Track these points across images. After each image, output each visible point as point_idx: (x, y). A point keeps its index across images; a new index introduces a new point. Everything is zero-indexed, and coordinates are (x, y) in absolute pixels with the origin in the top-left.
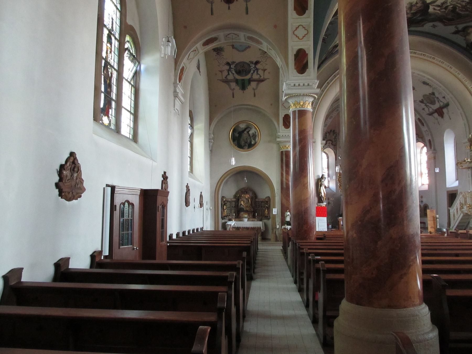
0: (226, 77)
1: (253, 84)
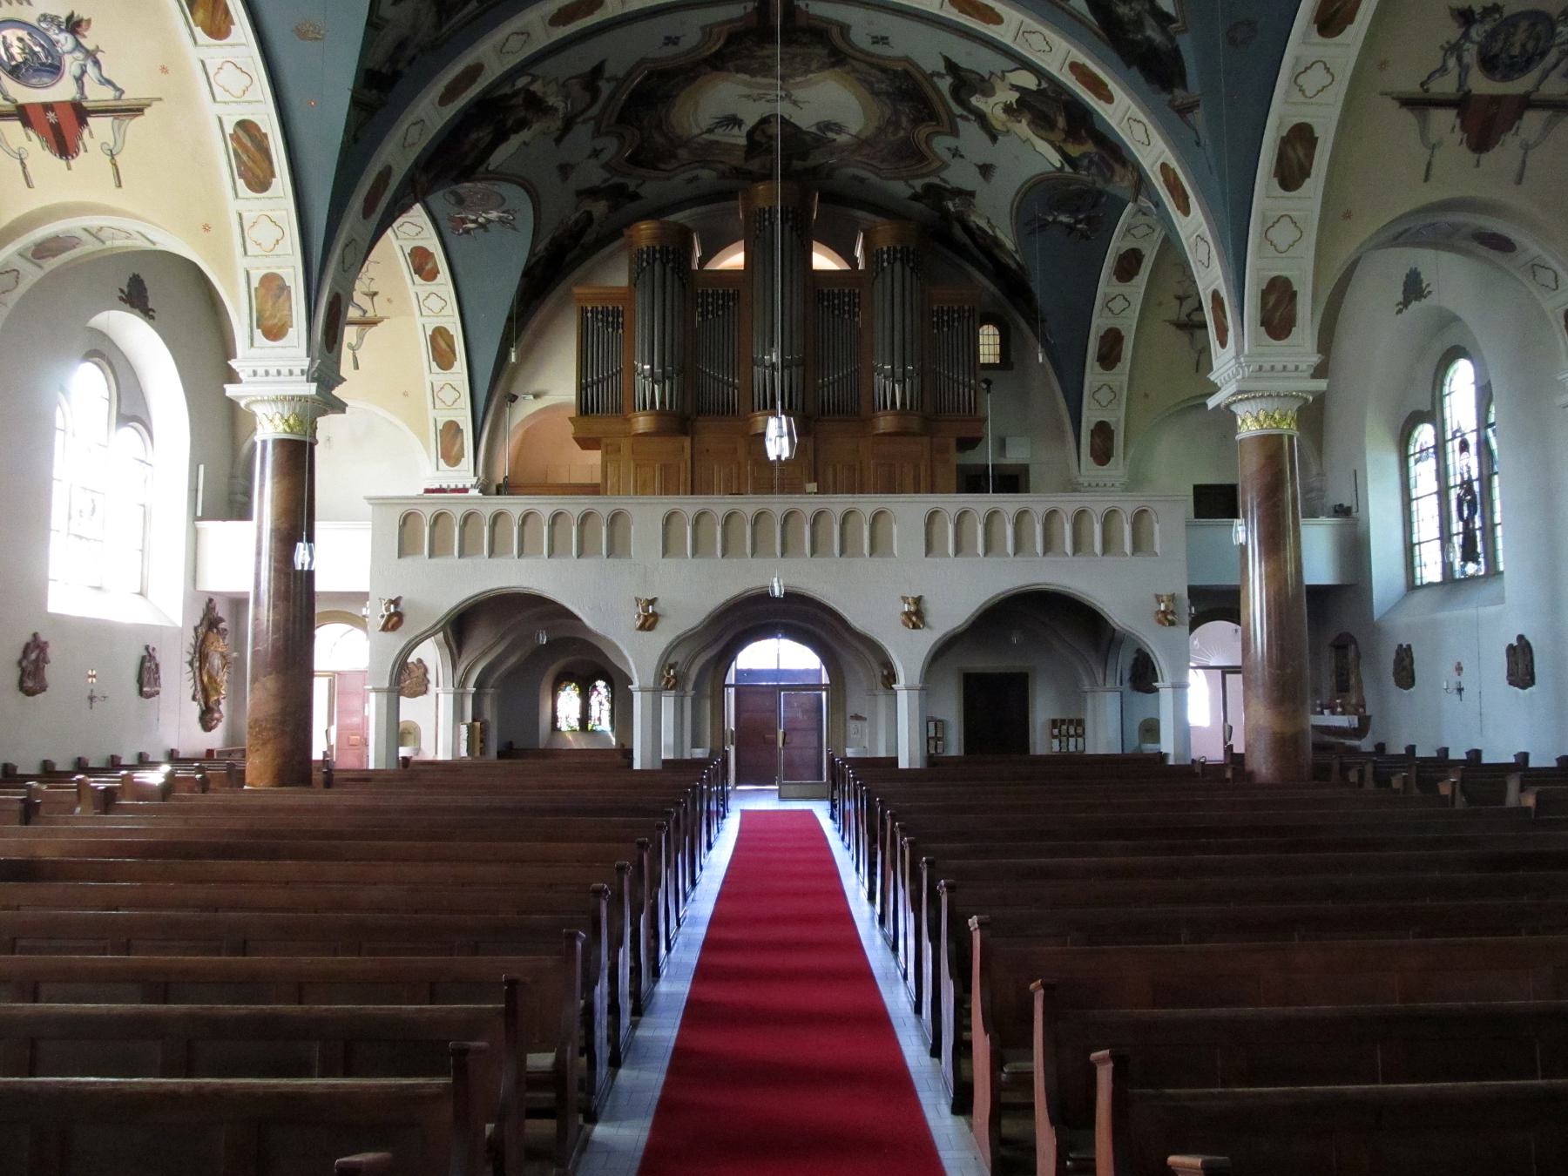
0: (1188, 315)
1: (99, 127)
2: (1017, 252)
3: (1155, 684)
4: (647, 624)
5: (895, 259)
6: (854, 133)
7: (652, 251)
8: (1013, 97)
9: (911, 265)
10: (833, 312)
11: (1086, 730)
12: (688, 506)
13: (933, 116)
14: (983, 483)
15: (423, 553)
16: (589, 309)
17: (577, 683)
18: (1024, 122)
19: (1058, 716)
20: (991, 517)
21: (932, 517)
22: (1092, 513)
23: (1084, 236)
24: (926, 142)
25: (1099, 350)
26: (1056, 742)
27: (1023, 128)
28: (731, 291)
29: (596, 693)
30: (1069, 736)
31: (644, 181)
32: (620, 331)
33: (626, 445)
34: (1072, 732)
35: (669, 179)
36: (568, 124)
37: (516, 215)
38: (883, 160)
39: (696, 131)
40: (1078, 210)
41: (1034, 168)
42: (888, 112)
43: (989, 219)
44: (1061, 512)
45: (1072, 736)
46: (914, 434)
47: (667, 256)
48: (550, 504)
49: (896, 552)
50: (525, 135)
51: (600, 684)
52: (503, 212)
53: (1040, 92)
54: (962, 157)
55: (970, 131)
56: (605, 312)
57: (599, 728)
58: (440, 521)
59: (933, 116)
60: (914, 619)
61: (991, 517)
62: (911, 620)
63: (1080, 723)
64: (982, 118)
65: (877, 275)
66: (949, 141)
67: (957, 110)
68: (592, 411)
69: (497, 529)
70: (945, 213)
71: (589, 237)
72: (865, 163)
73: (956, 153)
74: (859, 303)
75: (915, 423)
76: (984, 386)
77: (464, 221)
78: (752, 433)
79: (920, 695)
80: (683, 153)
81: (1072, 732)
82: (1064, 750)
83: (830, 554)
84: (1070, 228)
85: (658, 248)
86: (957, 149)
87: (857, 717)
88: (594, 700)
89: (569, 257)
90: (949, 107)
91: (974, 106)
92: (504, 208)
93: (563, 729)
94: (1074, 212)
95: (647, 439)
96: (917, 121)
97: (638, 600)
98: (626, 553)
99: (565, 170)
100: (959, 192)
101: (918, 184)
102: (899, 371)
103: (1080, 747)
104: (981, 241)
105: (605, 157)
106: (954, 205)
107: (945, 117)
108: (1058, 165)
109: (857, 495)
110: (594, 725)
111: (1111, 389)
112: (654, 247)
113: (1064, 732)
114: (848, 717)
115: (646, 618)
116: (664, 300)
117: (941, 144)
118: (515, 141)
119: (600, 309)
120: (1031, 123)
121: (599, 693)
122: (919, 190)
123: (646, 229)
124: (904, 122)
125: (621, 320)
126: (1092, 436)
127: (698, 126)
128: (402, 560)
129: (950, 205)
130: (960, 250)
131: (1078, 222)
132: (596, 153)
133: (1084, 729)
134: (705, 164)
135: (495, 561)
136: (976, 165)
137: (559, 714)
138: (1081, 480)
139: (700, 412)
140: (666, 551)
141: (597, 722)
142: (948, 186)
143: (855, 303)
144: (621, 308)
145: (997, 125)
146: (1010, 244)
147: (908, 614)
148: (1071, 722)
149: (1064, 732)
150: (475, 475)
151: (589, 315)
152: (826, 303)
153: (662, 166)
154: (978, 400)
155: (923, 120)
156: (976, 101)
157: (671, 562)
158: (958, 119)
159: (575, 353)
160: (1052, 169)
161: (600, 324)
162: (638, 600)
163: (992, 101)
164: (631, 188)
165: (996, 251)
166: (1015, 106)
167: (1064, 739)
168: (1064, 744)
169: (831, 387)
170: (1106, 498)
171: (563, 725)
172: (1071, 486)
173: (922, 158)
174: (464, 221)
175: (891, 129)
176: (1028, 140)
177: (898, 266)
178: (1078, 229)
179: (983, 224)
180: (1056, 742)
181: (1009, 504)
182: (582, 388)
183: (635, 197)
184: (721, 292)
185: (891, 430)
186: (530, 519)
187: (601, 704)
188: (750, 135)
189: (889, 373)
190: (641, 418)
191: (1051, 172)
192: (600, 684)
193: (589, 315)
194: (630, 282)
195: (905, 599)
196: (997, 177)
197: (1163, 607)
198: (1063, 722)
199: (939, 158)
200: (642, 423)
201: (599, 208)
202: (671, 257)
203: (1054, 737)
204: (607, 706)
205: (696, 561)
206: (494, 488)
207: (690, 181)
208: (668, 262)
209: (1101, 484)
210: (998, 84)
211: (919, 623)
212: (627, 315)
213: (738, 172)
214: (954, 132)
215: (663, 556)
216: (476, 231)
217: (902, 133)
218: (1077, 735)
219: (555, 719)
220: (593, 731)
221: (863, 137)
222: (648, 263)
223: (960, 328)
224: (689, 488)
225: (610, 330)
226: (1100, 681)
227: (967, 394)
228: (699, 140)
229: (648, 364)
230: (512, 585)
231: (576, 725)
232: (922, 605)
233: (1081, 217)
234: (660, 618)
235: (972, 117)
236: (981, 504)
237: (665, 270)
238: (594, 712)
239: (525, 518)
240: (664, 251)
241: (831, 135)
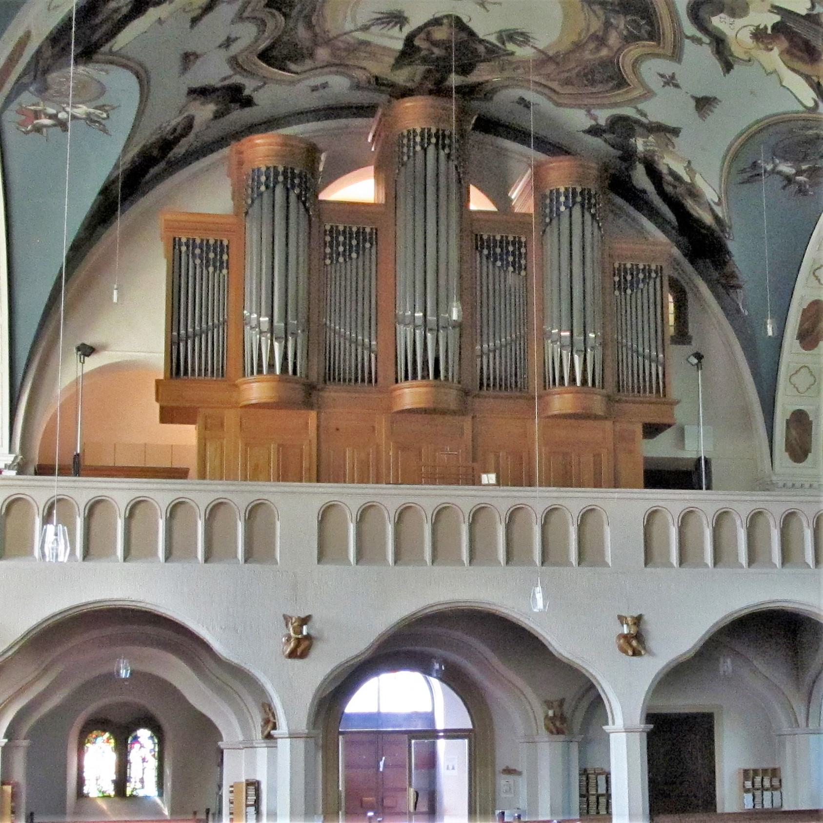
2: (719, 204)
3: (605, 727)
4: (299, 651)
5: (574, 203)
6: (541, 47)
9: (593, 211)
11: (783, 781)
13: (654, 35)
14: (695, 479)
15: (115, 553)
16: (184, 240)
17: (112, 733)
18: (776, 51)
19: (751, 766)
21: (326, 514)
22: (701, 514)
23: (802, 191)
25: (801, 325)
26: (748, 797)
28: (368, 230)
29: (137, 746)
30: (763, 789)
31: (265, 83)
32: (225, 271)
34: (767, 783)
35: (292, 83)
37: (111, 112)
38: (567, 82)
39: (348, 26)
40: (804, 159)
41: (784, 106)
43: (689, 162)
44: (769, 516)
45: (767, 790)
46: (596, 417)
47: (292, 180)
48: (170, 490)
49: (609, 559)
51: (144, 734)
52: (96, 108)
54: (677, 86)
56: (205, 246)
57: (141, 793)
58: (138, 512)
59: (654, 35)
60: (634, 643)
62: (631, 646)
63: (774, 773)
64: (719, 43)
65: (253, 202)
66: (666, 67)
67: (690, 29)
68: (186, 373)
71: (179, 150)
72: (541, 84)
73: (671, 81)
74: (526, 254)
75: (598, 405)
76: (695, 361)
77: (37, 115)
78: (396, 409)
79: (306, 743)
80: (323, 54)
81: (767, 783)
82: (758, 807)
83: (492, 560)
84: (789, 179)
85: (281, 169)
86: (673, 77)
87: (509, 771)
88: (135, 755)
89: (153, 171)
90: (680, 25)
91: (716, 28)
92: (100, 102)
93: (91, 795)
94: (797, 161)
95: (268, 412)
97: (287, 618)
98: (268, 556)
99: (704, 104)
101: (603, 116)
103: (777, 803)
104: (669, 189)
105: (235, 49)
106: (645, 144)
107: (669, 36)
108: (810, 104)
109: (304, 484)
110: (134, 789)
111: (811, 372)
112: (275, 168)
113: (758, 784)
114: (497, 772)
115: (299, 641)
119: (198, 241)
120: (789, 54)
121: (142, 746)
122: (602, 122)
123: (264, 145)
124: (613, 39)
125: (225, 257)
126: (788, 427)
127: (354, 19)
130: (635, 198)
131: (799, 173)
132: (228, 42)
133: (780, 781)
134: (338, 65)
135: (89, 564)
136: (693, 97)
137: (86, 775)
138: (774, 478)
139: (330, 376)
141: (139, 785)
142: (643, 119)
143: (520, 254)
144: (225, 243)
145: (737, 50)
146: (710, 194)
147: (626, 638)
148: (765, 771)
149: (758, 784)
150: (11, 451)
151: (184, 249)
152: (485, 252)
153: (292, 66)
154: (667, 380)
155: (638, 38)
156: (719, 22)
157: (329, 568)
158: (687, 41)
160: (801, 108)
161: (198, 261)
162: (287, 618)
163: (739, 22)
164: (247, 92)
165: (689, 203)
166: (769, 31)
167: (758, 793)
168: (758, 800)
169: (491, 355)
170: (754, 498)
171: (91, 789)
172: (763, 485)
173: (621, 83)
174: (37, 115)
175: (592, 46)
176: (775, 71)
177: (577, 210)
178: (796, 182)
179: (679, 169)
180: (748, 797)
182: (174, 344)
183: (248, 102)
184: (354, 229)
185: (570, 411)
186: (180, 512)
187: (144, 760)
188: (409, 40)
189: (567, 342)
190: (255, 385)
191: (797, 112)
192: (144, 734)
193: (184, 249)
194: (237, 207)
195: (622, 619)
197: (626, 630)
198: (756, 772)
199: (642, 84)
201: (204, 112)
202: (297, 181)
203: (747, 791)
204: (153, 763)
206: (32, 469)
207: (315, 89)
208: (293, 186)
209: (798, 485)
211: (640, 648)
212: (233, 250)
213: (378, 83)
214: (676, 55)
215: (319, 561)
216: (51, 130)
217: (604, 52)
218: (773, 788)
219: (81, 782)
220: (132, 796)
221: (551, 53)
222: (267, 187)
223: (645, 292)
224: (314, 476)
225: (211, 269)
226: (802, 719)
227: (366, 358)
228: (348, 38)
229: (266, 316)
230: (115, 597)
231: (111, 790)
232: (642, 626)
233: (804, 167)
234: (314, 642)
235: (706, 39)
237: (288, 198)
238: (135, 771)
239: (134, 508)
240: (289, 175)
241: (510, 47)
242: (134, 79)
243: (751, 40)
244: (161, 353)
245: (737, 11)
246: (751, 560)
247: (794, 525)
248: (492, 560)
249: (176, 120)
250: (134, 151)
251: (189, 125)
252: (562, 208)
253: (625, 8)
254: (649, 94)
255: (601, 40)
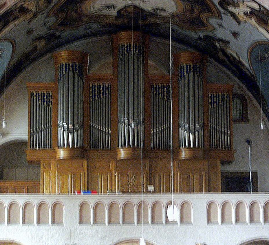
7: (68, 66)
8: (248, 10)
10: (159, 96)
12: (91, 199)
20: (239, 205)
21: (210, 205)
24: (207, 20)
27: (253, 21)
33: (53, 164)
36: (36, 14)
42: (188, 7)
49: (192, 222)
50: (17, 22)
53: (260, 11)
55: (227, 19)
59: (209, 10)
61: (239, 205)
64: (234, 15)
69: (11, 211)
70: (215, 47)
71: (33, 56)
73: (221, 25)
75: (201, 153)
80: (85, 19)
96: (202, 11)
98: (60, 223)
100: (220, 40)
102: (192, 128)
116: (74, 94)
117: (213, 21)
118: (12, 25)
128: (266, 224)
129: (218, 45)
140: (81, 222)
146: (247, 65)
157: (84, 227)
159: (27, 120)
165: (240, 66)
177: (191, 75)
179: (234, 55)
181: (246, 198)
183: (59, 37)
196: (240, 38)
200: (62, 154)
205: (111, 227)
210: (241, 4)
214: (220, 17)
236: (233, 198)
242: (11, 44)
243: (243, 15)
244: (26, 136)
245: (236, 5)
246: (223, 220)
247: (227, 207)
248: (146, 223)
249: (28, 49)
250: (14, 60)
251: (36, 47)
252: (185, 74)
253: (197, 2)
254: (215, 29)
255: (192, 11)
